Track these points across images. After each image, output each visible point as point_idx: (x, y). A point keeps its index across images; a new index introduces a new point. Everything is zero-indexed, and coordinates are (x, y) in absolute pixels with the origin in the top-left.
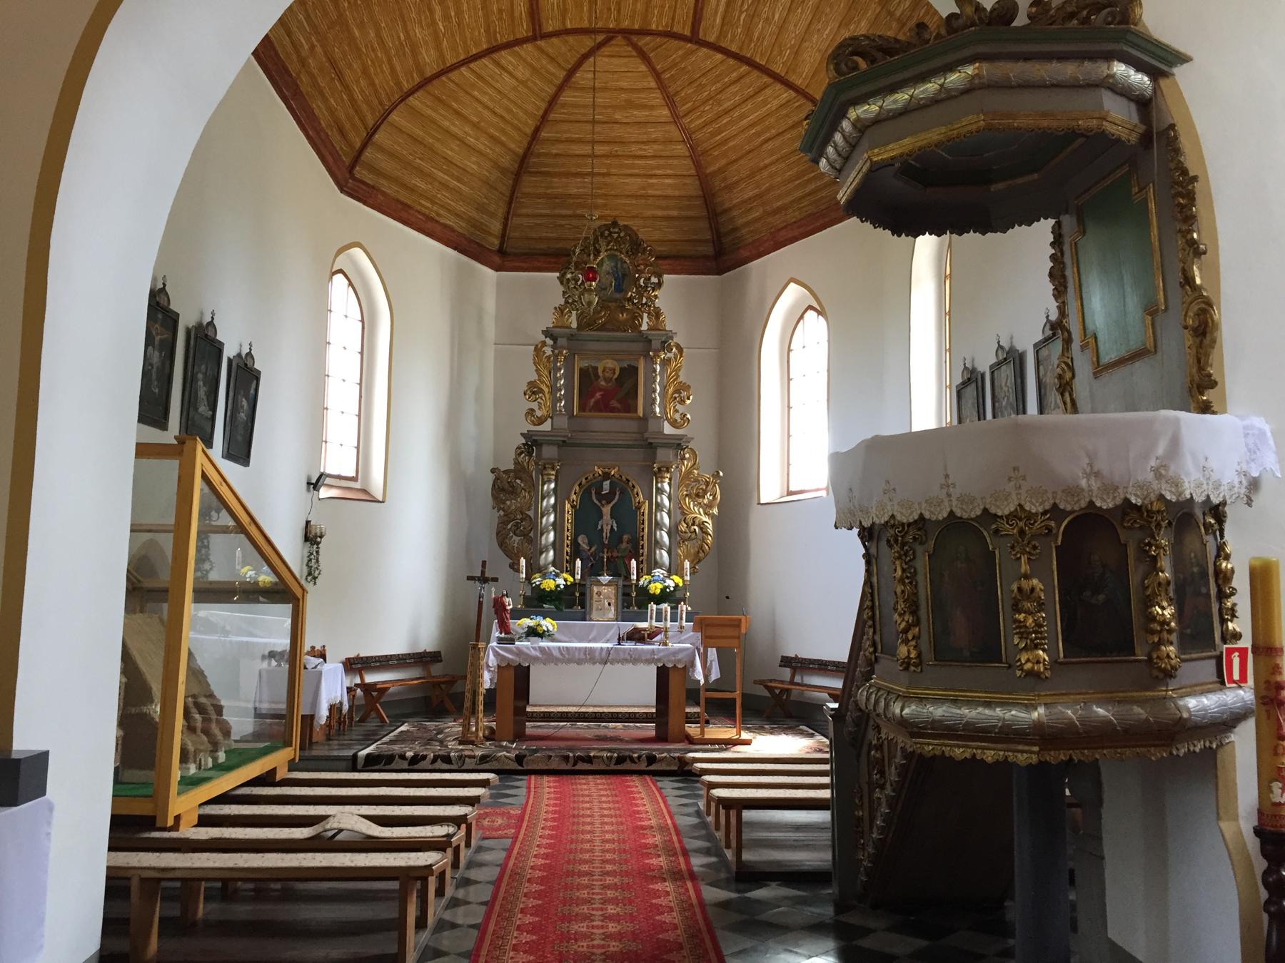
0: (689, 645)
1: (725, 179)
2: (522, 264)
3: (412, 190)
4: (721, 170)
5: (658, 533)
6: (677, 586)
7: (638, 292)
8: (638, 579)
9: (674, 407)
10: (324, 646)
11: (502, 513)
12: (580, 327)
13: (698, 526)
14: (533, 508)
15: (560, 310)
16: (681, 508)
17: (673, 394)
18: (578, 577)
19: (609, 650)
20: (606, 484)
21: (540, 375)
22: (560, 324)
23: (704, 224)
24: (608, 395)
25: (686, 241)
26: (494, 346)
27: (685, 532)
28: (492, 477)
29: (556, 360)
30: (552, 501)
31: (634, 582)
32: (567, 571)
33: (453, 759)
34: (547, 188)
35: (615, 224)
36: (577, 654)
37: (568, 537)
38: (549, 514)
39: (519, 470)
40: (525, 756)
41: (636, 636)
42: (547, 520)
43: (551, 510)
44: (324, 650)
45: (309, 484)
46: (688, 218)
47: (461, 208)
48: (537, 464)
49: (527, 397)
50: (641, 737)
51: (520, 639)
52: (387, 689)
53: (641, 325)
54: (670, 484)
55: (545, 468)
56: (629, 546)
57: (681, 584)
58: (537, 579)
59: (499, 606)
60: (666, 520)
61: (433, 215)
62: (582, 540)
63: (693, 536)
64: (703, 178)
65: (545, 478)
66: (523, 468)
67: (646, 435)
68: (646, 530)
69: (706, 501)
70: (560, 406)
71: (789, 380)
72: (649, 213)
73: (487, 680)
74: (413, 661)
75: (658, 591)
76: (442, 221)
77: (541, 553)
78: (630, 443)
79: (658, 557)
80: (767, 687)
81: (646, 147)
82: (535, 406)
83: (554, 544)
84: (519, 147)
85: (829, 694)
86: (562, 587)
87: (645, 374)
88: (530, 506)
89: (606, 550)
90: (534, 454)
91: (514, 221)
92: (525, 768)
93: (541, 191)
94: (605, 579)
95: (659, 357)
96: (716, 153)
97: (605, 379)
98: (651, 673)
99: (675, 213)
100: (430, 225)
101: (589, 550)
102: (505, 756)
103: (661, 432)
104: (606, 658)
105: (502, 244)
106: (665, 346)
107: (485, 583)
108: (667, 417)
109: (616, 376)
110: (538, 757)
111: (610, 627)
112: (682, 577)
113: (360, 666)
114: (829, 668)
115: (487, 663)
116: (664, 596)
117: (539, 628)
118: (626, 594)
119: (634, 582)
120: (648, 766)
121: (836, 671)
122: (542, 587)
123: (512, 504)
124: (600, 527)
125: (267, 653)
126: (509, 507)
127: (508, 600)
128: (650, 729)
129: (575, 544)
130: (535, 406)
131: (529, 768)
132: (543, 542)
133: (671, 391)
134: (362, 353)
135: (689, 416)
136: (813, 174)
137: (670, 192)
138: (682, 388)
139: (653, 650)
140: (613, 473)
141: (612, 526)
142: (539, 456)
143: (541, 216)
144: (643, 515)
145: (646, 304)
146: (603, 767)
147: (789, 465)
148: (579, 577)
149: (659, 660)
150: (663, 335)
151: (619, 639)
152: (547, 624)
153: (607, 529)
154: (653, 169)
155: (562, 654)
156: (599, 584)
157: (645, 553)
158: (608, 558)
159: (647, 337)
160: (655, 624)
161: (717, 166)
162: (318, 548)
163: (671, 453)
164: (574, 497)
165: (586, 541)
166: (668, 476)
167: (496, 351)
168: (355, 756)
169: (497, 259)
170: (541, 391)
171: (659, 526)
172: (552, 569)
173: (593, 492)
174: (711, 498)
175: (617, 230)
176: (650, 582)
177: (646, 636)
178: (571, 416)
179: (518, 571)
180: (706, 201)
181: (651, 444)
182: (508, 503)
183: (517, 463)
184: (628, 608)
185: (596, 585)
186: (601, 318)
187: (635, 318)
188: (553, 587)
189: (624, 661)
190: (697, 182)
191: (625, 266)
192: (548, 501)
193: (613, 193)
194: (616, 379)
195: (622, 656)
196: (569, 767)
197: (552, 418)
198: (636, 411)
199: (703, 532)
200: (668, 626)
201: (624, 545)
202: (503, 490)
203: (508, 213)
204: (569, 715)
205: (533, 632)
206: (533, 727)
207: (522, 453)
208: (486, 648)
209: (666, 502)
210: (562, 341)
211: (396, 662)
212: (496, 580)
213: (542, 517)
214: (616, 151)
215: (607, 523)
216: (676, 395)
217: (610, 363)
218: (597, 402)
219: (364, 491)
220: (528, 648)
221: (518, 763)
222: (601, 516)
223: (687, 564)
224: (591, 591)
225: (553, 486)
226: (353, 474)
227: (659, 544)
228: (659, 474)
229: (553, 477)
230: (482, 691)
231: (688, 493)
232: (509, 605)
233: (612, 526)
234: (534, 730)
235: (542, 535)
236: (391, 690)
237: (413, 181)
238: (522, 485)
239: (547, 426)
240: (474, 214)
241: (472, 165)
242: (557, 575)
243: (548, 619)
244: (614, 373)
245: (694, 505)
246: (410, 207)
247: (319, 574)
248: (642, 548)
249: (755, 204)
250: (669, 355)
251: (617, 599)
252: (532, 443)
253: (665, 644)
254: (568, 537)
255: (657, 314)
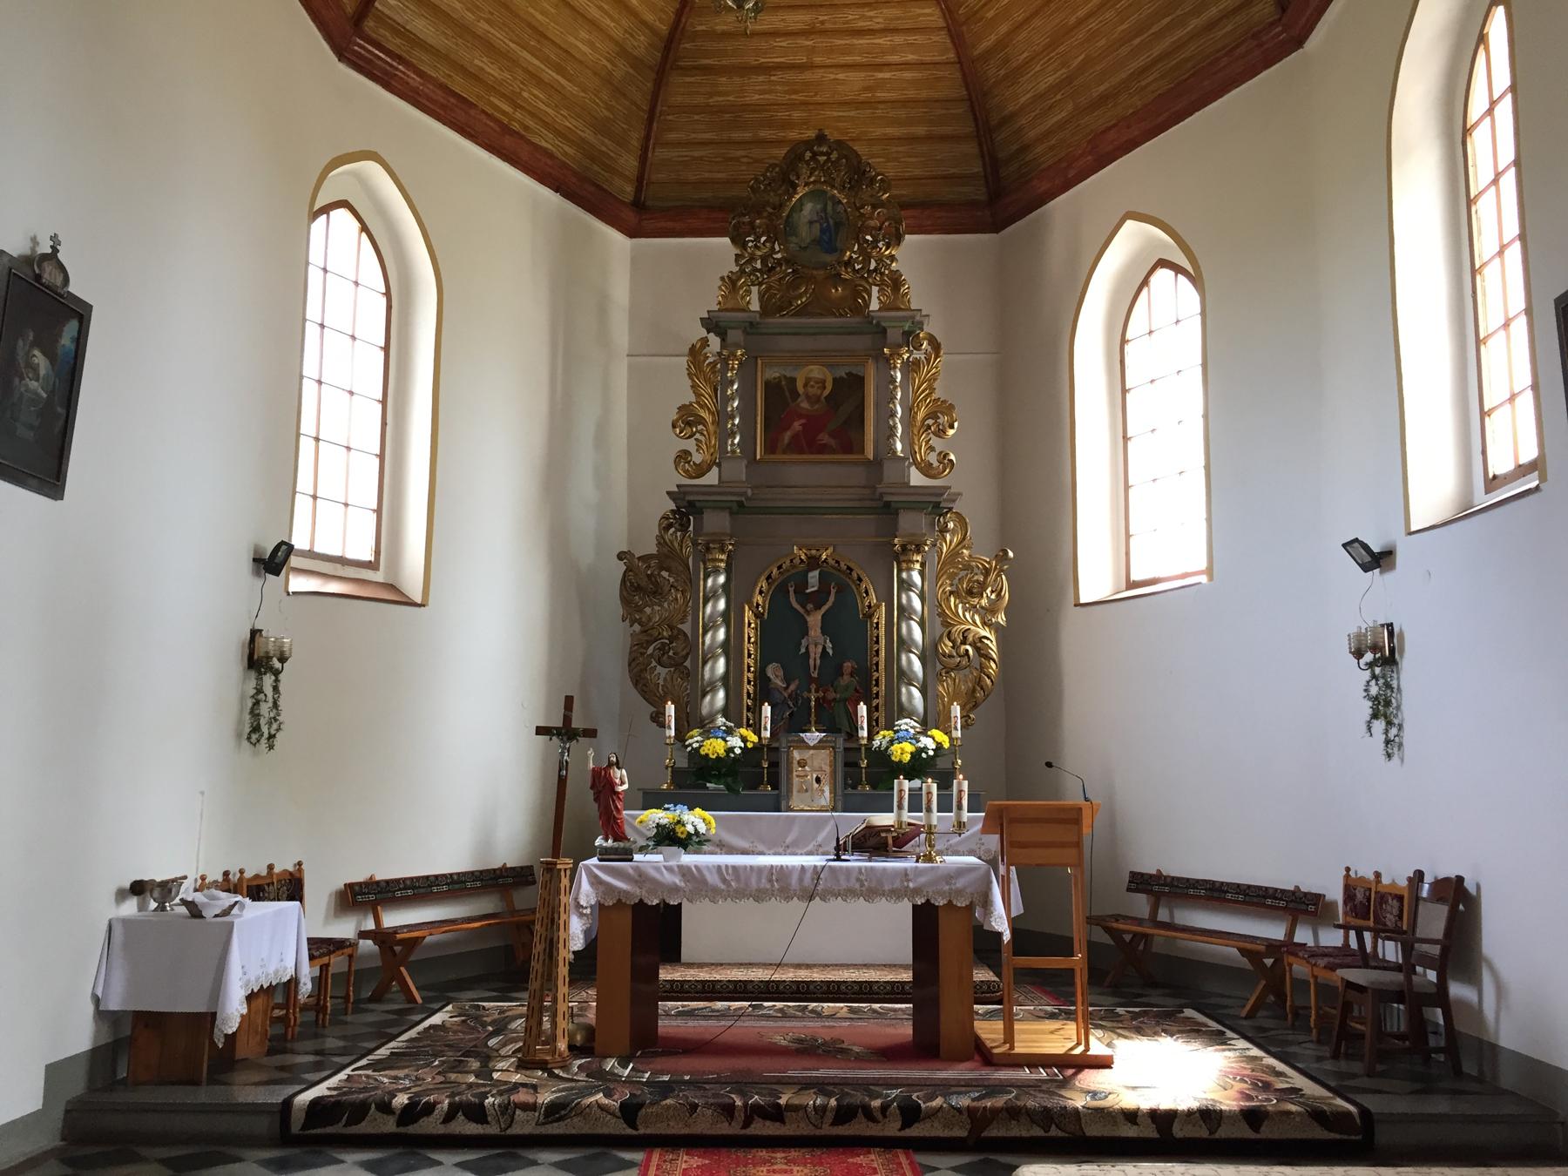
0: (973, 860)
1: (1006, 61)
2: (670, 224)
3: (474, 77)
4: (1001, 44)
5: (904, 658)
6: (939, 746)
7: (862, 251)
8: (871, 737)
9: (927, 442)
10: (300, 864)
11: (637, 627)
12: (766, 310)
13: (973, 644)
14: (690, 618)
15: (731, 282)
16: (942, 614)
17: (924, 420)
18: (767, 734)
19: (817, 872)
20: (814, 576)
21: (698, 395)
22: (729, 306)
23: (970, 148)
24: (813, 425)
25: (944, 177)
26: (626, 358)
27: (951, 656)
28: (621, 567)
29: (726, 368)
30: (722, 605)
31: (864, 742)
32: (748, 725)
33: (490, 1112)
34: (711, 95)
35: (821, 138)
36: (754, 881)
37: (749, 667)
38: (715, 628)
39: (666, 556)
40: (641, 1105)
41: (872, 843)
42: (713, 638)
43: (720, 620)
44: (300, 870)
45: (257, 561)
46: (943, 138)
47: (568, 122)
48: (695, 544)
49: (678, 430)
50: (882, 1042)
51: (642, 850)
52: (420, 939)
53: (867, 305)
54: (922, 573)
55: (708, 549)
56: (854, 680)
57: (946, 745)
58: (694, 739)
59: (602, 785)
60: (917, 634)
61: (516, 126)
62: (774, 672)
63: (965, 662)
64: (967, 65)
65: (710, 565)
66: (672, 549)
67: (881, 489)
68: (882, 653)
69: (984, 602)
70: (733, 444)
71: (1124, 391)
72: (878, 132)
73: (575, 932)
74: (478, 884)
75: (907, 758)
76: (536, 140)
77: (704, 695)
78: (857, 504)
79: (904, 699)
80: (1108, 930)
81: (871, 14)
82: (690, 445)
83: (725, 679)
84: (660, 20)
85: (1240, 950)
86: (738, 751)
87: (877, 389)
88: (685, 616)
89: (813, 687)
90: (691, 528)
91: (658, 154)
92: (642, 1131)
93: (700, 100)
94: (813, 737)
95: (900, 355)
96: (990, 15)
97: (808, 397)
98: (902, 914)
99: (921, 130)
100: (508, 141)
101: (786, 688)
102: (601, 1107)
103: (907, 484)
104: (812, 888)
105: (639, 190)
106: (910, 338)
107: (570, 739)
108: (915, 459)
109: (827, 392)
110: (669, 1107)
111: (821, 823)
112: (947, 733)
113: (372, 897)
114: (1229, 896)
115: (576, 899)
116: (918, 766)
117: (679, 829)
118: (851, 764)
119: (865, 742)
120: (902, 1128)
121: (1244, 902)
122: (702, 752)
123: (654, 612)
124: (803, 650)
125: (127, 885)
126: (650, 619)
127: (619, 774)
128: (898, 1022)
129: (762, 680)
130: (690, 445)
131: (649, 1131)
132: (707, 675)
133: (920, 416)
134: (386, 349)
135: (952, 457)
136: (1168, 19)
137: (911, 93)
138: (941, 409)
139: (906, 870)
140: (824, 557)
141: (824, 648)
142: (697, 531)
143: (703, 144)
144: (877, 628)
145: (875, 270)
146: (805, 1130)
147: (1128, 536)
148: (768, 734)
149: (916, 892)
150: (905, 319)
151: (838, 848)
152: (696, 819)
153: (815, 653)
154: (884, 53)
155: (724, 881)
156: (803, 745)
157: (882, 693)
158: (817, 700)
159: (878, 324)
160: (907, 817)
161: (993, 38)
162: (277, 680)
163: (923, 520)
164: (760, 599)
165: (781, 673)
166: (919, 558)
167: (630, 367)
168: (288, 1103)
169: (630, 216)
170: (702, 421)
171: (905, 644)
172: (721, 720)
173: (791, 590)
174: (993, 597)
175: (824, 149)
176: (891, 742)
177: (890, 841)
178: (752, 461)
179: (663, 725)
180: (972, 107)
181: (888, 505)
182: (648, 610)
183: (661, 542)
184: (854, 787)
185: (796, 748)
186: (800, 296)
187: (858, 294)
188: (722, 752)
189: (848, 894)
190: (958, 75)
191: (840, 208)
192: (714, 607)
193: (818, 98)
194: (826, 398)
195: (844, 884)
196: (733, 1129)
197: (719, 465)
198: (862, 451)
199: (981, 655)
200: (934, 822)
201: (846, 679)
202: (638, 588)
203: (647, 138)
204: (750, 987)
205: (668, 837)
206: (680, 1014)
207: (670, 526)
208: (574, 871)
209: (917, 603)
210: (735, 335)
211: (445, 888)
212: (591, 733)
213: (705, 633)
214: (822, 23)
215: (816, 642)
216: (930, 422)
217: (816, 371)
218: (795, 437)
219: (392, 587)
220: (657, 869)
221: (626, 1121)
222: (805, 632)
223: (956, 710)
224: (789, 754)
225: (722, 579)
226: (368, 556)
227: (905, 677)
228: (902, 557)
229: (723, 565)
230: (565, 955)
231: (954, 589)
232: (622, 783)
233: (824, 648)
234: (679, 1022)
235: (705, 663)
236: (428, 939)
237: (476, 62)
238: (672, 580)
239: (712, 478)
240: (588, 135)
241: (580, 42)
242: (729, 732)
243: (698, 810)
244: (825, 388)
245: (965, 610)
246: (472, 105)
247: (278, 730)
248: (877, 685)
249: (1059, 97)
250: (917, 355)
251: (834, 773)
252: (687, 508)
253: (929, 859)
254: (749, 667)
255: (896, 282)
